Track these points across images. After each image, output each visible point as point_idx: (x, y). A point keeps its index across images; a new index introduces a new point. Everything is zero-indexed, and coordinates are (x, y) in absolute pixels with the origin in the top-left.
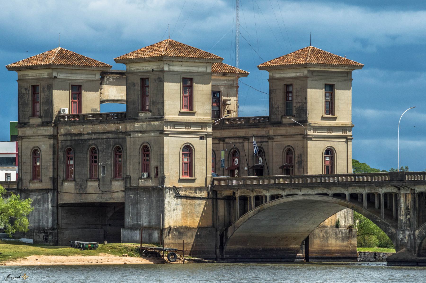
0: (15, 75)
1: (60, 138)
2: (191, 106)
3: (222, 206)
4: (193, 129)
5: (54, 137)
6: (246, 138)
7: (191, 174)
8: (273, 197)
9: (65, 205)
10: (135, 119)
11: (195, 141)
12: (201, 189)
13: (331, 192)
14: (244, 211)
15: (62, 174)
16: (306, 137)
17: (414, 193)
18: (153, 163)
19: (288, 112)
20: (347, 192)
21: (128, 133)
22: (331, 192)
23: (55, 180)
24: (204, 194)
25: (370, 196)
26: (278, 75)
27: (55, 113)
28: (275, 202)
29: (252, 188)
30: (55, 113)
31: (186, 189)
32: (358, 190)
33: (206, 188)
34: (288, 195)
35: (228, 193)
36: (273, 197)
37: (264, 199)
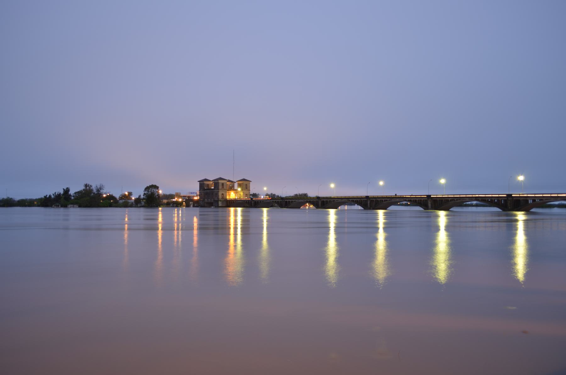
36: (337, 201)
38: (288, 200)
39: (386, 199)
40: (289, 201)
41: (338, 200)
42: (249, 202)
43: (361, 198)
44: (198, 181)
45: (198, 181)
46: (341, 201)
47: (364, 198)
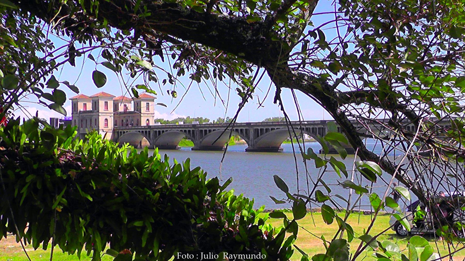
0: (91, 99)
1: (80, 117)
2: (107, 109)
3: (116, 134)
4: (108, 114)
5: (78, 117)
6: (129, 117)
7: (107, 126)
8: (272, 129)
9: (81, 134)
10: (94, 112)
11: (108, 118)
12: (110, 130)
13: (179, 130)
14: (121, 135)
15: (80, 126)
16: (99, 115)
17: (153, 131)
18: (97, 124)
19: (96, 109)
20: (187, 130)
21: (92, 116)
22: (179, 130)
23: (79, 127)
24: (111, 131)
25: (313, 129)
26: (94, 99)
27: (79, 111)
28: (215, 132)
29: (122, 129)
30: (79, 111)
31: (106, 130)
32: (143, 130)
33: (111, 130)
34: (277, 129)
35: (117, 131)
37: (315, 129)
38: (203, 129)
40: (206, 131)
41: (279, 128)
42: (143, 132)
44: (70, 99)
45: (70, 99)
46: (283, 129)
47: (318, 124)
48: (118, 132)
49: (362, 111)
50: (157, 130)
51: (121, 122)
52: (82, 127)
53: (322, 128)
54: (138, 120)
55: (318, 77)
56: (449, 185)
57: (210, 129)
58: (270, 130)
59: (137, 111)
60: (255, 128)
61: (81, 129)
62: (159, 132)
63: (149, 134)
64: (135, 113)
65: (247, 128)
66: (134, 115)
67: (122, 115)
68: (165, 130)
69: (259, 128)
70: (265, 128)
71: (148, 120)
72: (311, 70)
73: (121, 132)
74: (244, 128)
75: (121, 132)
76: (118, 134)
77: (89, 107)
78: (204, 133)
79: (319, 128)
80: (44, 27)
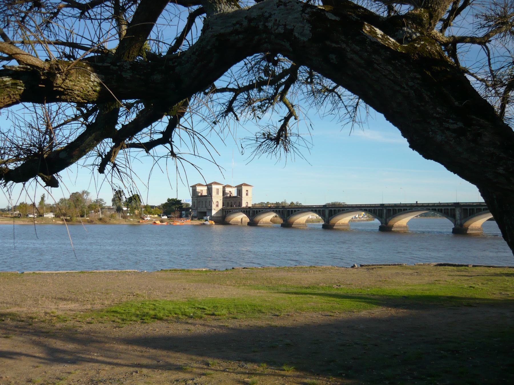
8: (298, 210)
23: (197, 207)
25: (374, 210)
38: (290, 210)
39: (405, 208)
42: (247, 211)
43: (447, 205)
48: (226, 211)
49: (97, 19)
50: (333, 209)
51: (227, 204)
52: (199, 207)
53: (381, 209)
54: (240, 202)
55: (19, 164)
56: (22, 133)
57: (295, 209)
58: (482, 210)
59: (239, 196)
60: (330, 209)
61: (199, 208)
62: (334, 210)
63: (249, 213)
64: (238, 197)
65: (323, 209)
66: (237, 199)
67: (227, 199)
68: (261, 210)
69: (333, 209)
70: (337, 209)
71: (247, 203)
72: (100, 37)
73: (228, 211)
74: (281, 210)
75: (228, 211)
76: (226, 213)
77: (234, 193)
78: (468, 211)
79: (379, 210)
80: (492, 66)
